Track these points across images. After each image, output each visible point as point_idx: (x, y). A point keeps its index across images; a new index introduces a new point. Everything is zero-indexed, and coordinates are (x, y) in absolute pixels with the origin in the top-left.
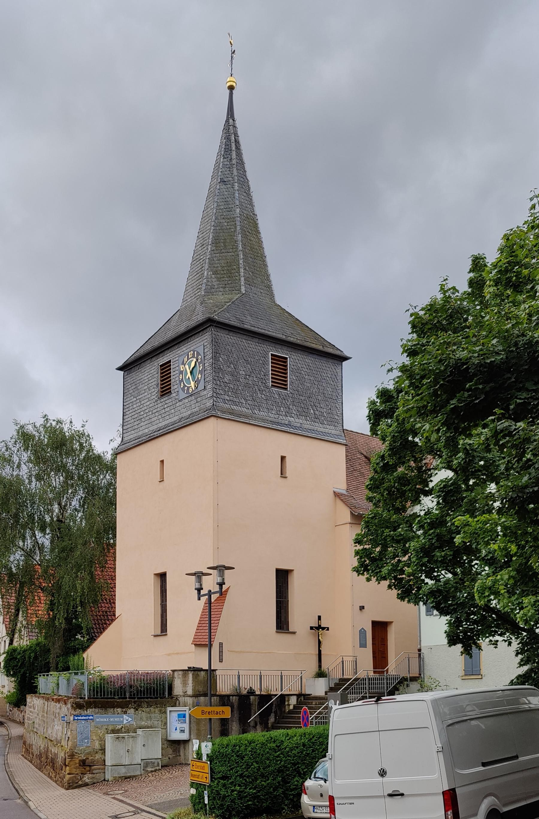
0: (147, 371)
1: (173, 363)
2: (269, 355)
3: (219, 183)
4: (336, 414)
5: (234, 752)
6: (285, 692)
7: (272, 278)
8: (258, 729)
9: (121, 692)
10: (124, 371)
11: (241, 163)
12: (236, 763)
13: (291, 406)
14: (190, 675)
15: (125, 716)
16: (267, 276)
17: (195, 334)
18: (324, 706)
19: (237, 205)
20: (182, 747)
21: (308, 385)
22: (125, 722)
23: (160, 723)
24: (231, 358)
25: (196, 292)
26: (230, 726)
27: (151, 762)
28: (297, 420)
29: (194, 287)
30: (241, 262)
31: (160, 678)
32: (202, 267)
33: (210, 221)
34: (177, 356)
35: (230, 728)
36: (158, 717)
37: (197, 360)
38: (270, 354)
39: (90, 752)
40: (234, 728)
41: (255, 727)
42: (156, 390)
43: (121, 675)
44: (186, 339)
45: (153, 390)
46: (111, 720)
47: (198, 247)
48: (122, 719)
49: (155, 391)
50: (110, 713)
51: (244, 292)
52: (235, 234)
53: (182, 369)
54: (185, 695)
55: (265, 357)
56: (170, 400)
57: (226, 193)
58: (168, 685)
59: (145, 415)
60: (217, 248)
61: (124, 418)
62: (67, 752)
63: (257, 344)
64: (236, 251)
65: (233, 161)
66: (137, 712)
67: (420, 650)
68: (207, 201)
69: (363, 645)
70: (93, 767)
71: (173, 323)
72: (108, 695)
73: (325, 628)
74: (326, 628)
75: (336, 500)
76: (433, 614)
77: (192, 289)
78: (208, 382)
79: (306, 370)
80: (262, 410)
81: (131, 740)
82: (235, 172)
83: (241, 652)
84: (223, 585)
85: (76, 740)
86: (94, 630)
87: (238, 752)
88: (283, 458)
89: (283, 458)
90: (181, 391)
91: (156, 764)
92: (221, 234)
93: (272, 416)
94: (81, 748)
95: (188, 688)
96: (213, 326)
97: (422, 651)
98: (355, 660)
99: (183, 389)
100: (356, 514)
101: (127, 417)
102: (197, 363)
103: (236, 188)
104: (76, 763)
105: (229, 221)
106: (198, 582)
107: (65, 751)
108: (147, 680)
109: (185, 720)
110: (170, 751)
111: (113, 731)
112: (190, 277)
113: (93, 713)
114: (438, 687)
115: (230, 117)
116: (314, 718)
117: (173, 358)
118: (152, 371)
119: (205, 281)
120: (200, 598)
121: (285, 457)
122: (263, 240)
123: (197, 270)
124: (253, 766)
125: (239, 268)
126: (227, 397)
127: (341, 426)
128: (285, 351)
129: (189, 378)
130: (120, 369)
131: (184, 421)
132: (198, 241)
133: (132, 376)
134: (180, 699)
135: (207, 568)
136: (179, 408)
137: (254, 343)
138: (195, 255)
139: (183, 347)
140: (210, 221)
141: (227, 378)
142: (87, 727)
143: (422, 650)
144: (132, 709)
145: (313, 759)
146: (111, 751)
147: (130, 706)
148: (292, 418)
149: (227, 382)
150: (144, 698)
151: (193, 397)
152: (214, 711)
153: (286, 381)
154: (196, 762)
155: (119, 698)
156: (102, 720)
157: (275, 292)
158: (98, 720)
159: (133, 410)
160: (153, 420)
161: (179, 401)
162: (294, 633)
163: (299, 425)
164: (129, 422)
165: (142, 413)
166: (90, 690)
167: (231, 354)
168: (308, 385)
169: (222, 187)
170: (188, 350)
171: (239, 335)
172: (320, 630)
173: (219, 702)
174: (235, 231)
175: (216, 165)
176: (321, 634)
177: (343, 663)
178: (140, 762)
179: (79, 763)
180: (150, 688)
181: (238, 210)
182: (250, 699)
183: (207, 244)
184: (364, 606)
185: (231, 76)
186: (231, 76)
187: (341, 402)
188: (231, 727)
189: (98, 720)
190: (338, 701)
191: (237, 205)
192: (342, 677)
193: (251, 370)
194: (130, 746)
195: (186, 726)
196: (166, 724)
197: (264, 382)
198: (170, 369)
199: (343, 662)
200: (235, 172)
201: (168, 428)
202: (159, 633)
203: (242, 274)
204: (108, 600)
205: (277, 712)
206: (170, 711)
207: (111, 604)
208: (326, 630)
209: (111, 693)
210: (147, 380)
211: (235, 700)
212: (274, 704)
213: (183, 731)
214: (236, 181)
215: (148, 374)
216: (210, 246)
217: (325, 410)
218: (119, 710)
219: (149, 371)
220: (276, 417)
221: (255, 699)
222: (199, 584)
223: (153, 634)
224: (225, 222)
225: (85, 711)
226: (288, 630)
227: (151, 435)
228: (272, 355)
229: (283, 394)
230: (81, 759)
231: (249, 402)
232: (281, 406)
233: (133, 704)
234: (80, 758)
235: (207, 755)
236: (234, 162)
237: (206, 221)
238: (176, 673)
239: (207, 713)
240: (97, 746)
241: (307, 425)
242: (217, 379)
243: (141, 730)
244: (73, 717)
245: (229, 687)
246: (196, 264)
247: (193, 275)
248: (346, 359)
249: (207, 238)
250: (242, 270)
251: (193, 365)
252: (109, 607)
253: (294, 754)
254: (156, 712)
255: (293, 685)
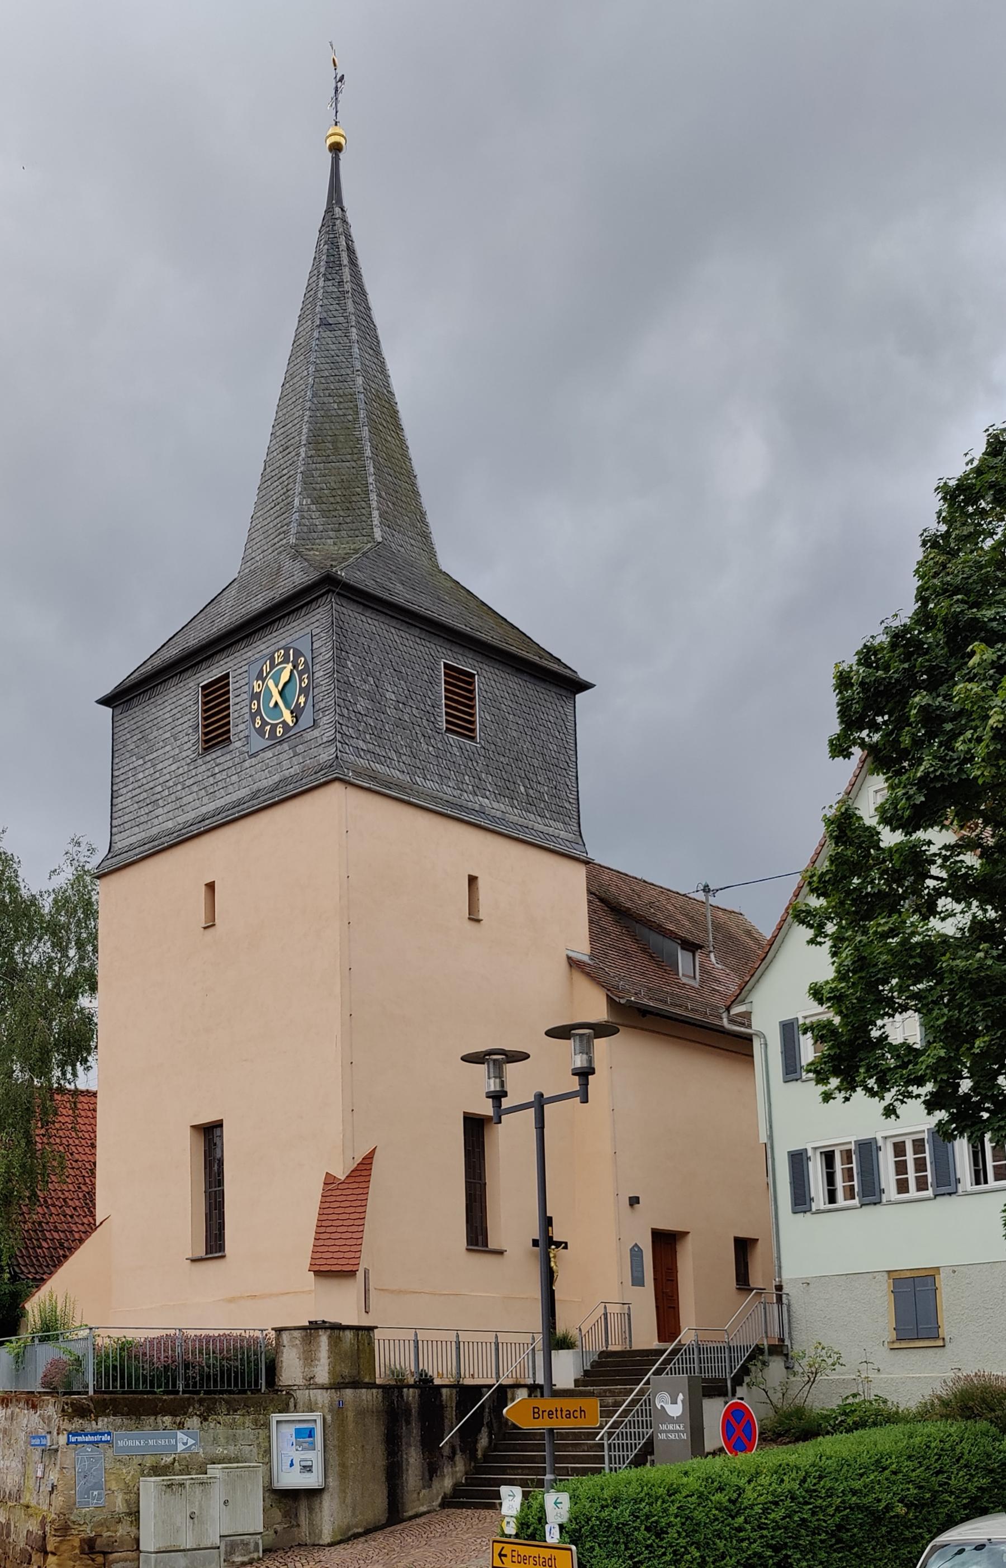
0: (170, 702)
1: (235, 680)
2: (440, 665)
3: (319, 326)
4: (566, 798)
5: (638, 1517)
6: (504, 1381)
7: (430, 519)
8: (457, 1463)
9: (167, 1378)
10: (113, 708)
11: (360, 292)
12: (647, 1547)
13: (483, 776)
14: (323, 1339)
15: (180, 1434)
16: (421, 516)
17: (289, 614)
18: (621, 1409)
19: (358, 371)
20: (303, 1505)
21: (515, 734)
22: (181, 1447)
23: (255, 1450)
24: (369, 663)
25: (276, 540)
26: (405, 1456)
27: (242, 1540)
28: (495, 805)
29: (270, 532)
30: (371, 479)
31: (249, 1349)
32: (288, 491)
33: (301, 400)
34: (245, 662)
35: (404, 1461)
36: (252, 1437)
37: (295, 667)
38: (442, 664)
39: (106, 1519)
40: (412, 1461)
41: (452, 1458)
42: (194, 738)
43: (159, 1339)
44: (266, 626)
45: (186, 739)
46: (151, 1442)
47: (275, 454)
48: (173, 1442)
49: (191, 739)
50: (148, 1427)
51: (380, 540)
52: (356, 426)
53: (256, 690)
54: (310, 1383)
55: (433, 668)
56: (228, 755)
57: (333, 347)
58: (266, 1363)
59: (166, 793)
60: (319, 453)
61: (114, 803)
62: (49, 1520)
63: (418, 641)
64: (359, 459)
65: (345, 286)
66: (205, 1423)
67: (779, 1288)
68: (292, 365)
69: (638, 1281)
70: (112, 1557)
71: (226, 603)
72: (137, 1384)
73: (561, 1243)
74: (563, 1243)
75: (571, 975)
76: (811, 1210)
77: (266, 535)
78: (323, 710)
79: (510, 703)
80: (429, 778)
81: (198, 1489)
82: (351, 307)
83: (400, 1292)
84: (590, 1077)
85: (73, 1492)
86: (17, 1260)
87: (648, 1517)
88: (472, 880)
89: (472, 880)
90: (254, 734)
91: (252, 1546)
92: (327, 427)
93: (449, 791)
94: (84, 1511)
95: (319, 1368)
96: (334, 592)
97: (785, 1290)
98: (626, 1312)
99: (261, 732)
100: (623, 1001)
101: (121, 799)
102: (295, 672)
103: (354, 336)
104: (74, 1548)
105: (342, 400)
106: (495, 1077)
107: (44, 1518)
108: (221, 1351)
109: (313, 1443)
110: (277, 1514)
111: (157, 1470)
112: (259, 514)
113: (110, 1427)
114: (837, 1366)
115: (336, 203)
116: (606, 1434)
117: (235, 667)
118: (184, 700)
119: (296, 516)
120: (500, 1118)
121: (476, 878)
122: (409, 443)
123: (274, 497)
124: (688, 1557)
125: (367, 492)
126: (362, 744)
127: (575, 825)
128: (470, 661)
129: (276, 703)
130: (105, 701)
131: (266, 797)
132: (274, 442)
133: (134, 715)
134: (299, 1394)
135: (464, 1059)
136: (252, 771)
137: (412, 637)
138: (268, 470)
139: (258, 643)
140: (301, 400)
141: (362, 704)
142: (97, 1461)
143: (784, 1287)
144: (195, 1417)
145: (814, 1534)
146: (155, 1516)
147: (190, 1410)
148: (486, 800)
149: (363, 713)
150: (221, 1392)
151: (286, 746)
152: (561, 1411)
153: (473, 723)
154: (514, 1547)
155: (165, 1393)
156: (130, 1443)
157: (438, 548)
158: (120, 1443)
159: (136, 785)
160: (184, 801)
161: (251, 756)
162: (500, 1253)
163: (499, 814)
164: (127, 810)
165: (159, 789)
166: (99, 1373)
167: (369, 655)
168: (515, 734)
169: (324, 335)
170: (272, 648)
171: (382, 618)
172: (553, 1247)
173: (383, 1401)
174: (356, 420)
175: (308, 296)
176: (555, 1257)
177: (606, 1319)
178: (217, 1541)
179: (81, 1547)
180: (229, 1370)
181: (360, 380)
182: (441, 1395)
183: (296, 446)
184: (638, 1198)
185: (336, 125)
186: (336, 125)
187: (574, 774)
188: (407, 1459)
189: (120, 1443)
190: (681, 1395)
191: (358, 371)
192: (605, 1349)
193: (406, 692)
194: (197, 1503)
195: (315, 1457)
196: (268, 1451)
197: (433, 719)
198: (228, 692)
199: (605, 1314)
200: (351, 307)
201: (224, 814)
202: (201, 1252)
203: (374, 504)
204: (42, 1200)
205: (492, 1424)
206: (278, 1422)
207: (47, 1207)
208: (563, 1248)
209: (144, 1382)
210: (170, 720)
211: (414, 1397)
212: (487, 1406)
213: (307, 1469)
214: (353, 324)
215: (173, 706)
216: (303, 450)
217: (546, 788)
218: (168, 1419)
219: (175, 699)
220: (456, 795)
221: (451, 1394)
222: (498, 1080)
223: (190, 1256)
224: (335, 402)
225: (94, 1422)
226: (486, 1244)
227: (183, 831)
228: (446, 665)
229: (468, 748)
230: (86, 1536)
231: (404, 757)
232: (464, 771)
233: (197, 1406)
234: (83, 1535)
235: (561, 1527)
236: (348, 287)
237: (290, 402)
238: (285, 1336)
239: (546, 1414)
240: (119, 1504)
241: (514, 816)
242: (343, 705)
243: (220, 1466)
244: (66, 1436)
245: (383, 1369)
246: (272, 487)
247: (266, 510)
248: (584, 686)
249: (296, 433)
250: (373, 496)
251: (285, 677)
252: (44, 1214)
253: (773, 1521)
254: (247, 1425)
255: (522, 1362)
